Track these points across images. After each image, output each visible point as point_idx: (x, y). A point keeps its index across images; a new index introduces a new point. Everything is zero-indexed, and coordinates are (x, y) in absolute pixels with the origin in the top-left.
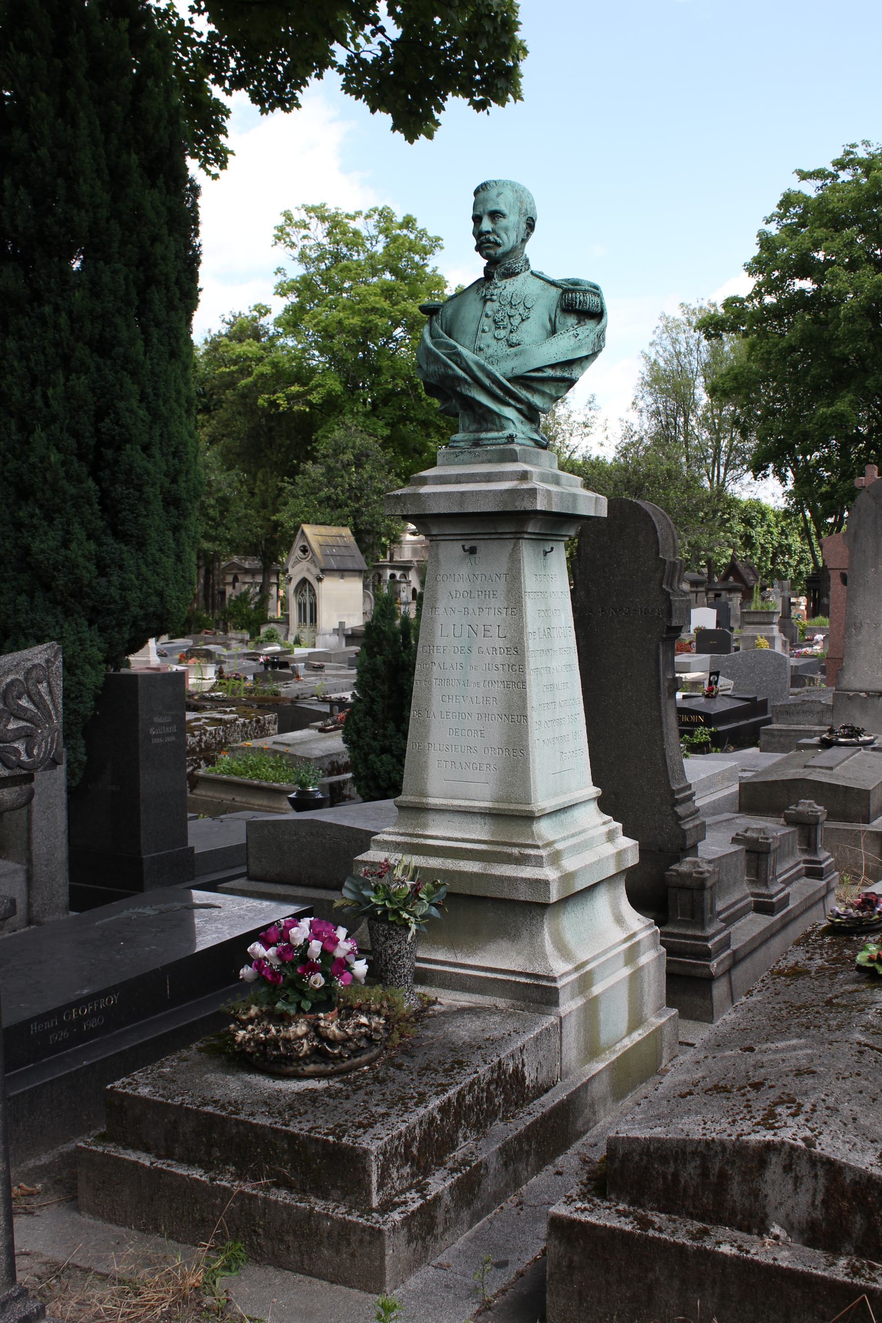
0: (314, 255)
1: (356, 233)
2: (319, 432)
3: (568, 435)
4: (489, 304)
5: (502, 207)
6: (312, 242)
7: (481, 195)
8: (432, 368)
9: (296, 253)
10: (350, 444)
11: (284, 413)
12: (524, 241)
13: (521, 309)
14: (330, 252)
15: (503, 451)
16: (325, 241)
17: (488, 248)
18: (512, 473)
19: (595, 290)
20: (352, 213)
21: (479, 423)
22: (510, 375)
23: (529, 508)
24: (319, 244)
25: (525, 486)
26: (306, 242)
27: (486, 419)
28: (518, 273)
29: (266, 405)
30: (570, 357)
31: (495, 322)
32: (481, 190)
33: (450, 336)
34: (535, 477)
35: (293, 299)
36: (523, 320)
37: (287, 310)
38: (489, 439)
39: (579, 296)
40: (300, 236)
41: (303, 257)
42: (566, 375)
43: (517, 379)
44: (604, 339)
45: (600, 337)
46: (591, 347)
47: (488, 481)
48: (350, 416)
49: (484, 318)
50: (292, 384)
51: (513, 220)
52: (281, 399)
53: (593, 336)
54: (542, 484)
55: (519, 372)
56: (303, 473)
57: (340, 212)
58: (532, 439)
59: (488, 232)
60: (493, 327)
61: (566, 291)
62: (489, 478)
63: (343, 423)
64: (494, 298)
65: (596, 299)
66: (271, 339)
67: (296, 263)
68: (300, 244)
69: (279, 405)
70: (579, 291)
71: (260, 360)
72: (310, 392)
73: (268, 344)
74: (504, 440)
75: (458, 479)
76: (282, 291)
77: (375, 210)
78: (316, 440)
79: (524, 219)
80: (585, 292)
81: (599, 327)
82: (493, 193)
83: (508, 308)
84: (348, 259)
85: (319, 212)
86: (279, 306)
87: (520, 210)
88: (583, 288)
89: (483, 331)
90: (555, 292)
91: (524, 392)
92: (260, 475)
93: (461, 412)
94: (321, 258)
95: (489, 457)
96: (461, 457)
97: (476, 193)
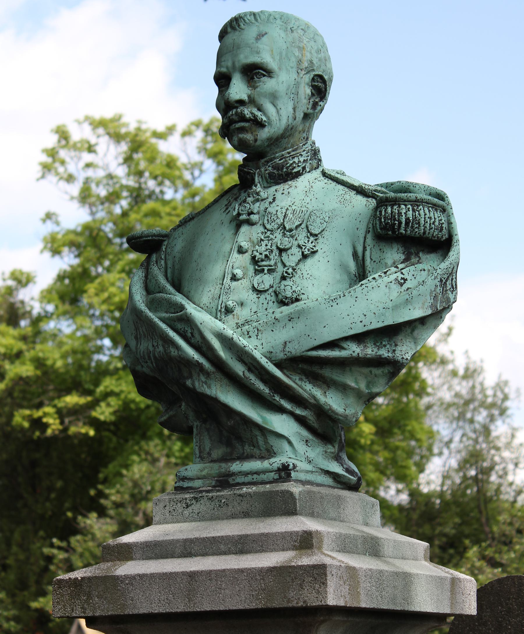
0: (103, 192)
1: (171, 163)
2: (111, 467)
3: (511, 467)
4: (244, 229)
5: (266, 58)
6: (101, 173)
7: (230, 38)
8: (145, 346)
9: (75, 189)
10: (158, 486)
11: (54, 438)
12: (309, 117)
13: (302, 237)
14: (127, 188)
15: (270, 495)
16: (121, 171)
17: (242, 130)
18: (284, 536)
19: (438, 201)
20: (161, 128)
21: (228, 444)
22: (281, 356)
23: (313, 602)
24: (110, 176)
25: (306, 561)
26: (90, 173)
27: (239, 437)
28: (298, 175)
29: (26, 424)
30: (389, 321)
31: (254, 261)
32: (231, 29)
33: (179, 288)
34: (326, 542)
35: (68, 261)
36: (305, 257)
37: (61, 278)
38: (246, 474)
39: (406, 212)
40: (82, 164)
41: (85, 197)
42: (384, 353)
43: (294, 363)
44: (454, 288)
45: (448, 285)
46: (429, 301)
47: (242, 552)
48: (157, 441)
49: (235, 255)
50: (68, 391)
51: (285, 83)
52: (49, 417)
53: (432, 283)
54: (341, 557)
55: (296, 349)
56: (83, 532)
57: (144, 127)
58: (328, 473)
59: (241, 102)
60: (251, 269)
61: (383, 202)
62: (241, 545)
63: (147, 453)
64: (254, 218)
65: (437, 215)
66: (36, 321)
67: (76, 204)
68: (81, 176)
69: (46, 426)
70: (406, 201)
71: (16, 356)
72: (95, 404)
73: (29, 331)
74: (273, 476)
75: (188, 549)
76: (54, 246)
77: (198, 124)
78: (105, 481)
79: (307, 78)
80: (417, 203)
81: (443, 265)
82: (250, 33)
83: (278, 235)
84: (157, 199)
85: (111, 128)
86: (47, 270)
87: (300, 62)
88: (412, 196)
89: (234, 278)
90: (362, 205)
91: (308, 387)
92: (17, 536)
94: (113, 198)
95: (245, 506)
96: (196, 507)
97: (223, 35)
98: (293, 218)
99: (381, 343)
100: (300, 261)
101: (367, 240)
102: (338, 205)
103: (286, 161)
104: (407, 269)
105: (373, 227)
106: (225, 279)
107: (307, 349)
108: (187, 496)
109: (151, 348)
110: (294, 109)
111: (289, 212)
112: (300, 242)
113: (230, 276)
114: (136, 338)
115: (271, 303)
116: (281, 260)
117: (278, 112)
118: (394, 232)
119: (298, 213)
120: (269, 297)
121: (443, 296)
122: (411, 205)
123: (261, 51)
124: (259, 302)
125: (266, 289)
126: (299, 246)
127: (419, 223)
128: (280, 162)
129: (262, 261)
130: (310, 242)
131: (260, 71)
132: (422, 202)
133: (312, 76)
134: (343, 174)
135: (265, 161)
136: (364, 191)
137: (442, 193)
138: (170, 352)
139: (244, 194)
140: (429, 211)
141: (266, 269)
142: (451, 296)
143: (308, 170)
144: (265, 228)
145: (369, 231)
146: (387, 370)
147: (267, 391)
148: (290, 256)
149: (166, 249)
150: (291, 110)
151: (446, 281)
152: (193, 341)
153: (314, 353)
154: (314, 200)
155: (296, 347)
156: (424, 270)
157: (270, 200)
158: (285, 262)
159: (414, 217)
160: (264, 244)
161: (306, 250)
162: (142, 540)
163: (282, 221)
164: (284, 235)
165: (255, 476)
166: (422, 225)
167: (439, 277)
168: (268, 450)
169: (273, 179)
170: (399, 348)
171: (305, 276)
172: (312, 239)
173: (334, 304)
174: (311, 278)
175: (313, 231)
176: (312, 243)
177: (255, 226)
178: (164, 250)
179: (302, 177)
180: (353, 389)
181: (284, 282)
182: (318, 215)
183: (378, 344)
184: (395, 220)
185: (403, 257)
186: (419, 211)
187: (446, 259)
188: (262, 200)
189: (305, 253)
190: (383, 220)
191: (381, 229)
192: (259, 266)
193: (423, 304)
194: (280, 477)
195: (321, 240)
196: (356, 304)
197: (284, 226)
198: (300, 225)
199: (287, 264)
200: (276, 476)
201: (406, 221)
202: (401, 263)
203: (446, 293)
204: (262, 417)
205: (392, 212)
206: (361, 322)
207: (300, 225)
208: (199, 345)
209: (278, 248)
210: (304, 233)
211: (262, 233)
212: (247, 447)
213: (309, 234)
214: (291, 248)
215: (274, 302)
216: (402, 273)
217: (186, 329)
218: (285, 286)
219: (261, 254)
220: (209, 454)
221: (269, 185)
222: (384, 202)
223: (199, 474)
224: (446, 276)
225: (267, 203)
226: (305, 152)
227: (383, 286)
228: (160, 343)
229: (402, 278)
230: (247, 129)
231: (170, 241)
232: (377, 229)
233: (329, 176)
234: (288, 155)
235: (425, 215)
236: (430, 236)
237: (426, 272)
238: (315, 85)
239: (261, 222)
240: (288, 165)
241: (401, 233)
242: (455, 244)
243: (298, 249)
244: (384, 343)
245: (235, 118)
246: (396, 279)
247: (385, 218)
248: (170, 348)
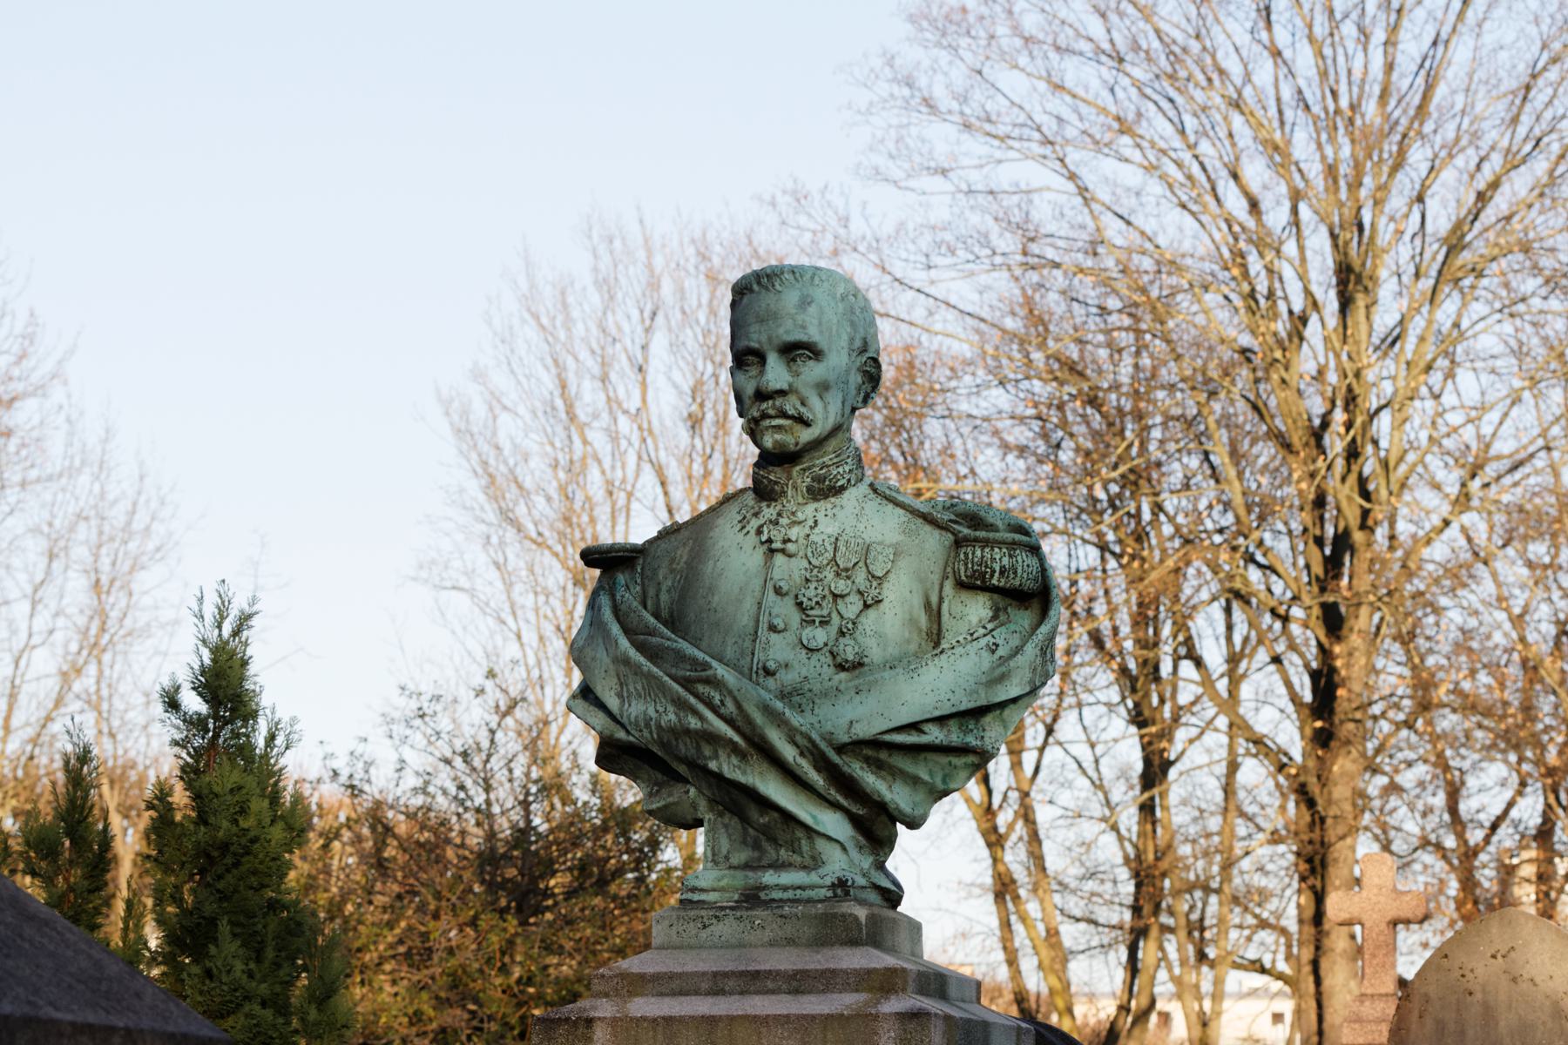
4: (779, 559)
5: (813, 334)
21: (756, 846)
28: (843, 489)
36: (866, 606)
38: (785, 888)
42: (972, 740)
46: (1028, 675)
47: (796, 992)
55: (864, 731)
62: (798, 983)
64: (791, 547)
74: (824, 893)
93: (708, 816)
95: (789, 930)
102: (902, 537)
108: (703, 913)
118: (983, 581)
126: (860, 593)
146: (971, 759)
147: (821, 782)
152: (722, 711)
153: (887, 738)
157: (811, 522)
160: (813, 586)
162: (966, 971)
164: (838, 575)
165: (798, 892)
168: (813, 858)
170: (987, 734)
172: (875, 584)
180: (925, 783)
181: (841, 640)
194: (835, 895)
195: (885, 585)
200: (830, 894)
204: (814, 817)
212: (782, 852)
220: (727, 858)
223: (715, 885)
227: (972, 653)
228: (671, 708)
245: (771, 412)
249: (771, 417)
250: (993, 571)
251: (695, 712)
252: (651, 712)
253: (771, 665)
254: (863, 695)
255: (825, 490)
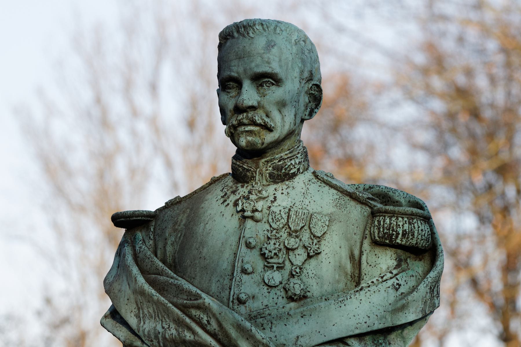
5: (275, 68)
16: (240, 188)
28: (294, 175)
31: (263, 255)
36: (309, 257)
46: (421, 306)
59: (253, 108)
64: (257, 215)
87: (302, 72)
89: (244, 271)
98: (297, 221)
99: (378, 341)
100: (305, 261)
101: (364, 245)
103: (285, 163)
104: (401, 275)
105: (371, 234)
106: (235, 272)
107: (317, 344)
109: (160, 330)
110: (295, 116)
111: (292, 213)
112: (304, 242)
113: (239, 269)
114: (137, 316)
115: (280, 298)
116: (289, 259)
117: (283, 118)
118: (391, 241)
119: (300, 215)
120: (278, 293)
121: (431, 302)
122: (407, 218)
123: (272, 61)
124: (269, 296)
125: (276, 285)
126: (305, 247)
127: (413, 235)
128: (280, 163)
129: (272, 258)
130: (314, 244)
131: (270, 80)
132: (416, 216)
133: (311, 85)
134: (332, 177)
135: (266, 161)
136: (359, 198)
137: (421, 203)
138: (185, 336)
139: (242, 189)
140: (421, 223)
141: (275, 266)
142: (436, 302)
143: (301, 171)
144: (271, 226)
145: (366, 237)
148: (297, 256)
149: (154, 229)
150: (292, 116)
151: (434, 288)
154: (312, 202)
155: (307, 342)
156: (413, 276)
157: (271, 198)
158: (292, 261)
159: (410, 229)
160: (272, 242)
161: (312, 251)
163: (286, 221)
164: (290, 235)
166: (415, 237)
167: (429, 285)
169: (273, 179)
171: (311, 275)
172: (315, 241)
173: (343, 305)
174: (315, 277)
175: (316, 234)
176: (316, 244)
177: (260, 223)
178: (152, 230)
179: (297, 177)
181: (292, 280)
182: (319, 218)
183: (376, 342)
184: (393, 230)
185: (395, 263)
186: (414, 224)
187: (434, 268)
188: (264, 198)
189: (311, 254)
190: (382, 230)
191: (379, 237)
192: (269, 263)
193: (416, 309)
195: (323, 242)
196: (360, 305)
197: (289, 226)
198: (304, 226)
199: (295, 263)
201: (403, 232)
202: (394, 269)
203: (433, 299)
205: (390, 224)
206: (366, 323)
207: (304, 226)
208: (215, 333)
209: (285, 247)
210: (307, 234)
211: (268, 231)
213: (312, 236)
214: (297, 248)
215: (283, 298)
216: (397, 279)
217: (201, 316)
218: (295, 284)
219: (270, 251)
221: (268, 183)
222: (383, 213)
224: (434, 284)
225: (269, 202)
226: (300, 154)
227: (382, 291)
228: (173, 326)
229: (397, 284)
230: (256, 132)
231: (159, 223)
232: (375, 237)
233: (322, 179)
234: (286, 157)
235: (419, 227)
236: (420, 246)
237: (414, 278)
238: (312, 94)
239: (265, 220)
240: (287, 166)
241: (398, 243)
242: (441, 254)
243: (304, 250)
244: (380, 341)
245: (245, 121)
246: (393, 285)
247: (383, 227)
248: (185, 332)
249: (245, 125)
250: (398, 234)
251: (190, 329)
252: (159, 328)
253: (243, 297)
254: (307, 317)
255: (281, 176)
